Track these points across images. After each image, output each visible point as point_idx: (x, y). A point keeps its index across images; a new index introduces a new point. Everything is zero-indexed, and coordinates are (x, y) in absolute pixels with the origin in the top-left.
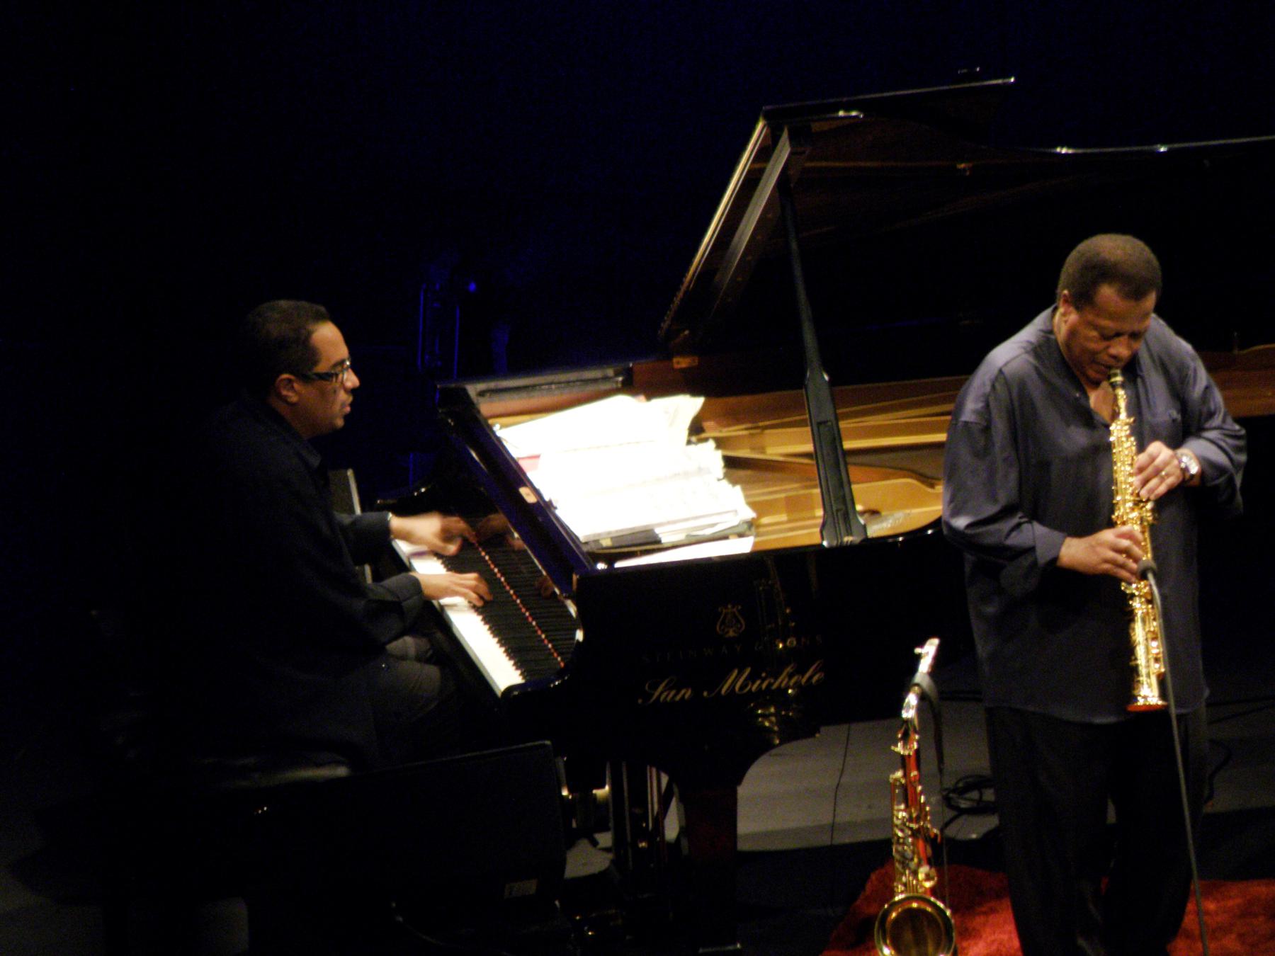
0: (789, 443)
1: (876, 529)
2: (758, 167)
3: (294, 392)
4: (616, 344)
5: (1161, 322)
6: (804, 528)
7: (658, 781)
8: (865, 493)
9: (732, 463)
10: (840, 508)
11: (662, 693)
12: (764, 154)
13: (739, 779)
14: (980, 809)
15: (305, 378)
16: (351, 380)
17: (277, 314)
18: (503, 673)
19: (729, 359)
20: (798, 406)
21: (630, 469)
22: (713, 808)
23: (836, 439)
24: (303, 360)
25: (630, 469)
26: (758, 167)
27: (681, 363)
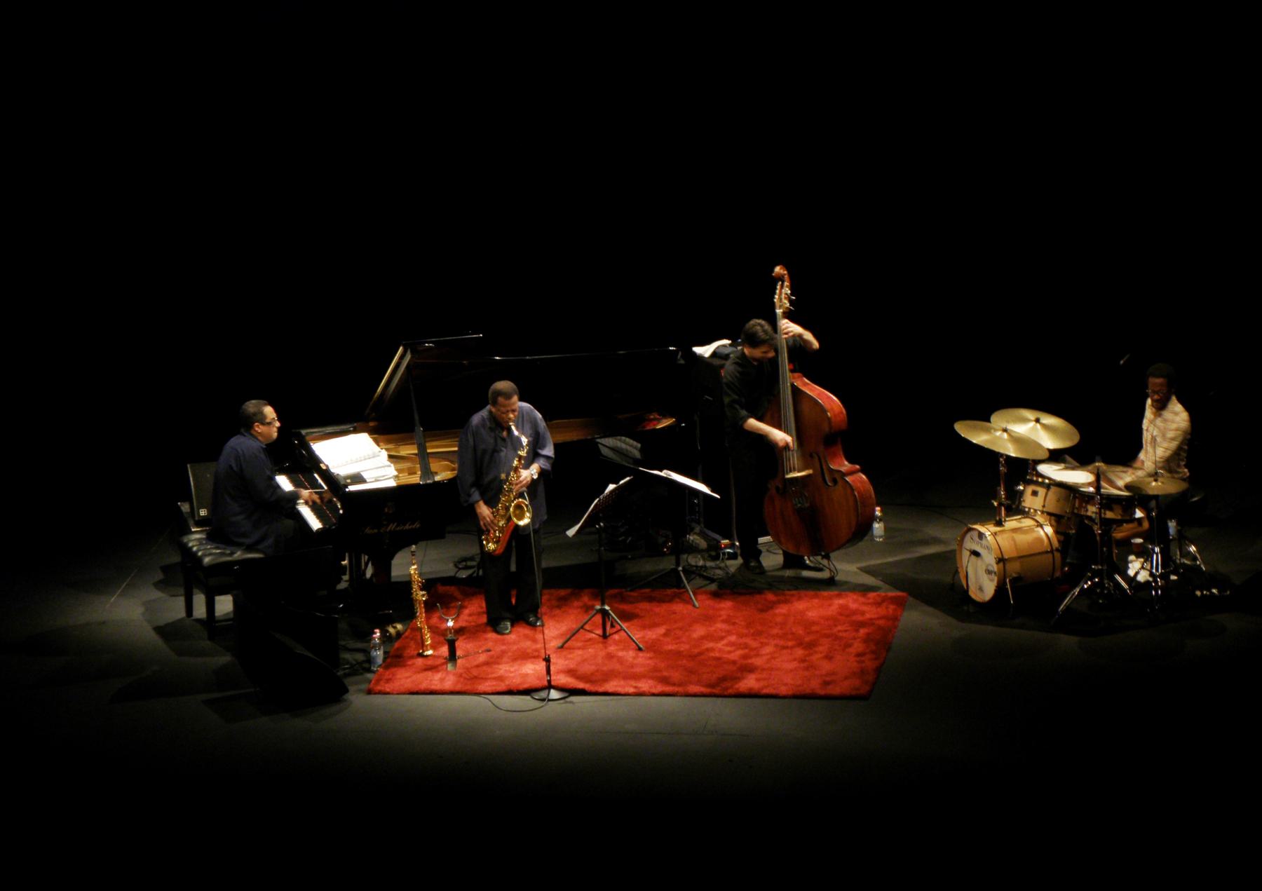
0: (409, 450)
1: (437, 478)
2: (400, 360)
3: (259, 428)
4: (343, 419)
5: (1145, 426)
6: (416, 479)
7: (365, 558)
8: (434, 466)
9: (390, 457)
10: (427, 472)
11: (368, 531)
12: (402, 357)
13: (392, 558)
14: (467, 568)
15: (263, 424)
16: (278, 424)
17: (251, 406)
18: (315, 524)
19: (387, 425)
20: (412, 438)
21: (358, 458)
22: (384, 567)
23: (425, 449)
24: (262, 420)
25: (358, 458)
26: (400, 360)
27: (371, 424)
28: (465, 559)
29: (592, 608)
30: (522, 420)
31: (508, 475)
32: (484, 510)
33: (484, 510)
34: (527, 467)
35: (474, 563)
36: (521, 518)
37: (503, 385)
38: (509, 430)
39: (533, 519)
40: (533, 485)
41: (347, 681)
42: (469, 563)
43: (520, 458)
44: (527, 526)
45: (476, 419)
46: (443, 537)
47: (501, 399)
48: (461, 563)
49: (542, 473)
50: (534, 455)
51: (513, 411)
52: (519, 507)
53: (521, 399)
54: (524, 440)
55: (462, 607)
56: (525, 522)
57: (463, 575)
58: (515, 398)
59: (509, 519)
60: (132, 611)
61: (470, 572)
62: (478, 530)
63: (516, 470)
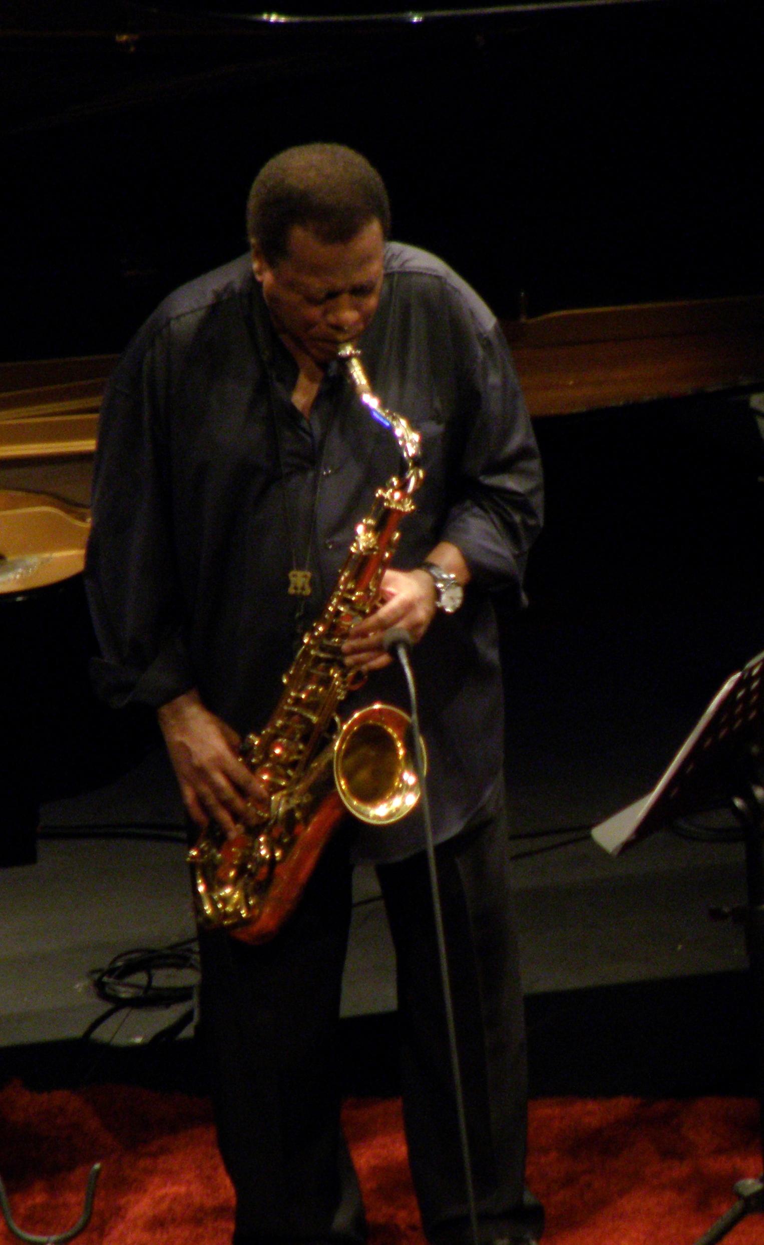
14: (152, 999)
28: (148, 960)
29: (725, 1186)
30: (411, 336)
31: (325, 586)
32: (201, 736)
33: (201, 736)
34: (412, 557)
35: (190, 978)
36: (374, 793)
37: (315, 165)
38: (337, 389)
39: (431, 787)
40: (441, 636)
41: (42, 846)
42: (163, 978)
43: (385, 519)
44: (414, 817)
45: (189, 304)
46: (28, 857)
47: (301, 236)
48: (123, 976)
49: (479, 582)
50: (452, 487)
51: (361, 291)
52: (371, 738)
53: (394, 233)
54: (408, 438)
55: (121, 1184)
56: (400, 802)
57: (135, 1030)
58: (374, 229)
59: (324, 788)
60: (256, 743)
61: (164, 1018)
62: (165, 817)
63: (365, 567)
